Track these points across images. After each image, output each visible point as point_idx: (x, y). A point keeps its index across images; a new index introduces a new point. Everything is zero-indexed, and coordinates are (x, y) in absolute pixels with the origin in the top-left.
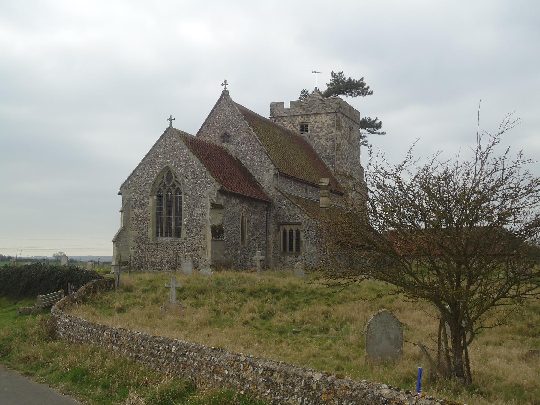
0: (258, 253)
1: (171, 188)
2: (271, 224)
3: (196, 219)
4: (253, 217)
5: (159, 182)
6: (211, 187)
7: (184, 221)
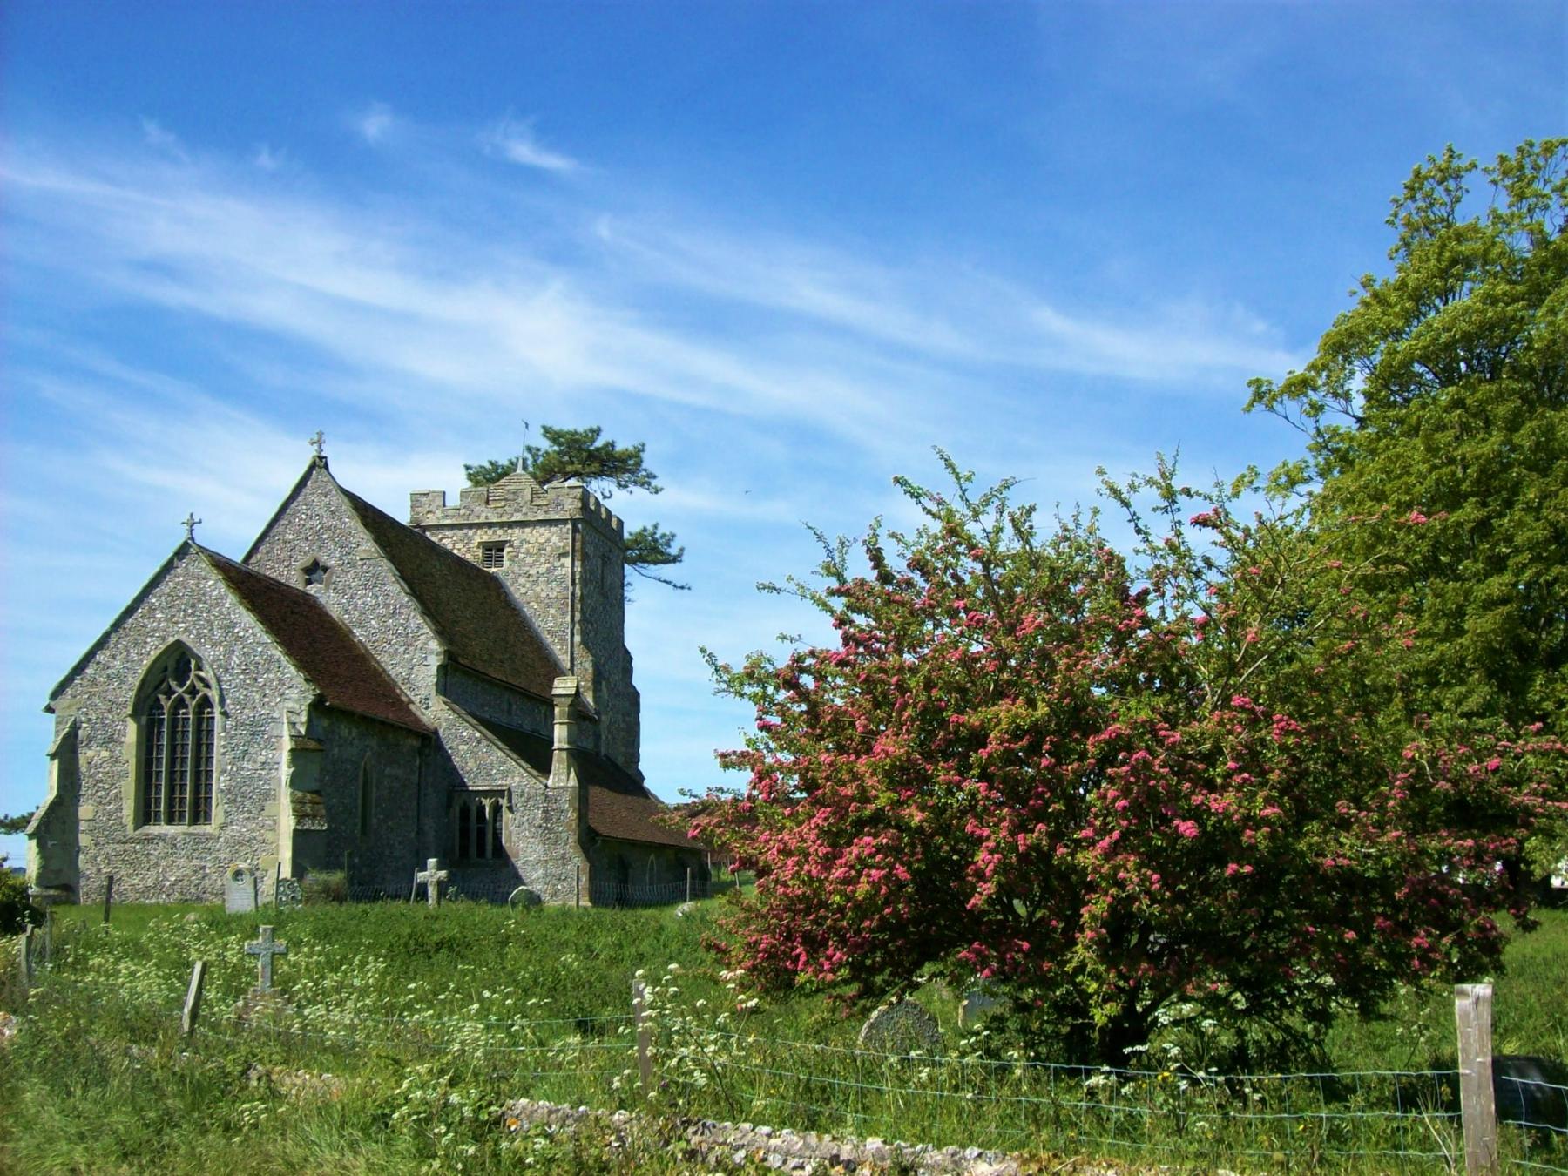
0: (432, 861)
1: (187, 697)
3: (250, 778)
4: (388, 771)
6: (294, 694)
7: (219, 782)
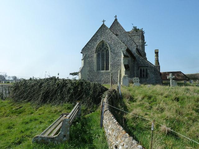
2: (135, 67)
5: (98, 47)
